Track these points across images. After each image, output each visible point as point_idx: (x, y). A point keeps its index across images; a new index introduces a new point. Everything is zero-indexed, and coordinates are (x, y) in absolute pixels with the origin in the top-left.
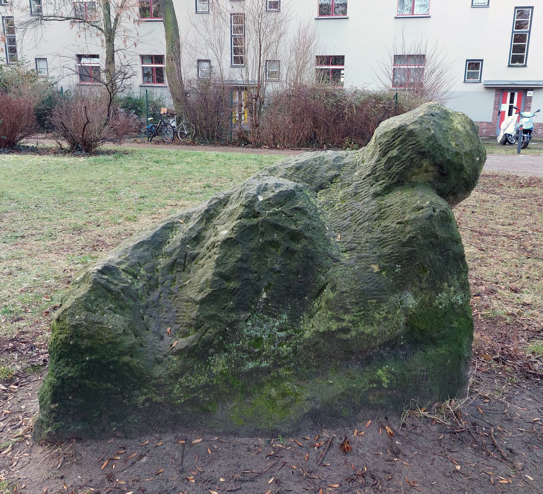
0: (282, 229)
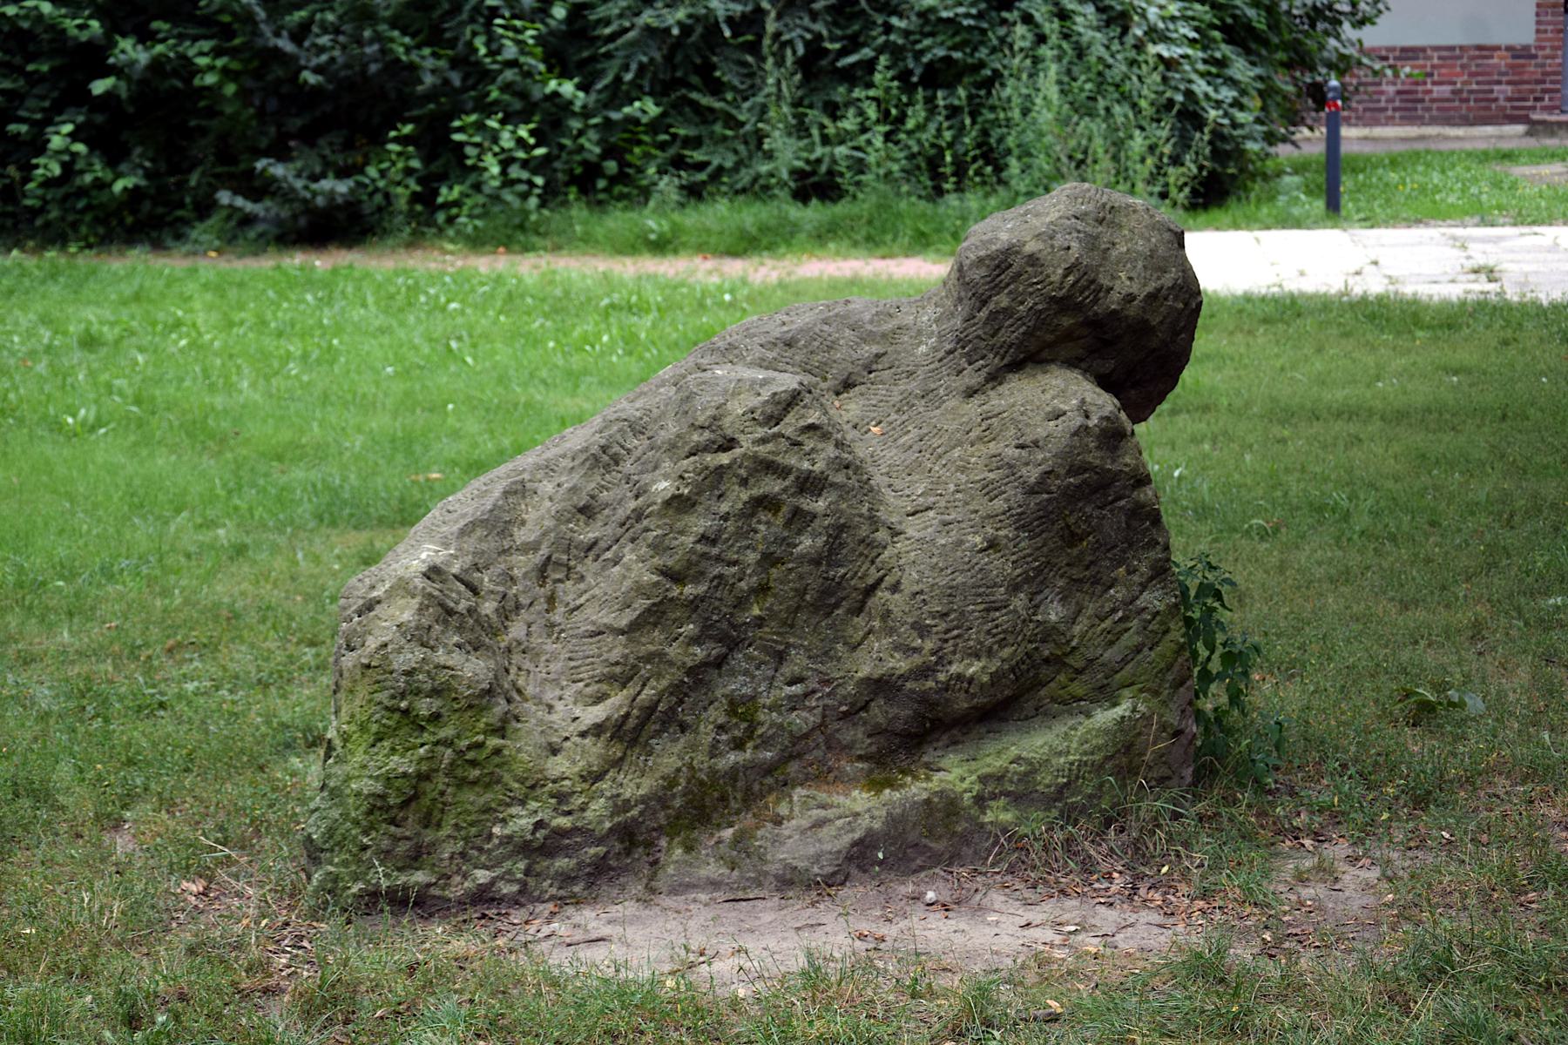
0: (784, 472)
